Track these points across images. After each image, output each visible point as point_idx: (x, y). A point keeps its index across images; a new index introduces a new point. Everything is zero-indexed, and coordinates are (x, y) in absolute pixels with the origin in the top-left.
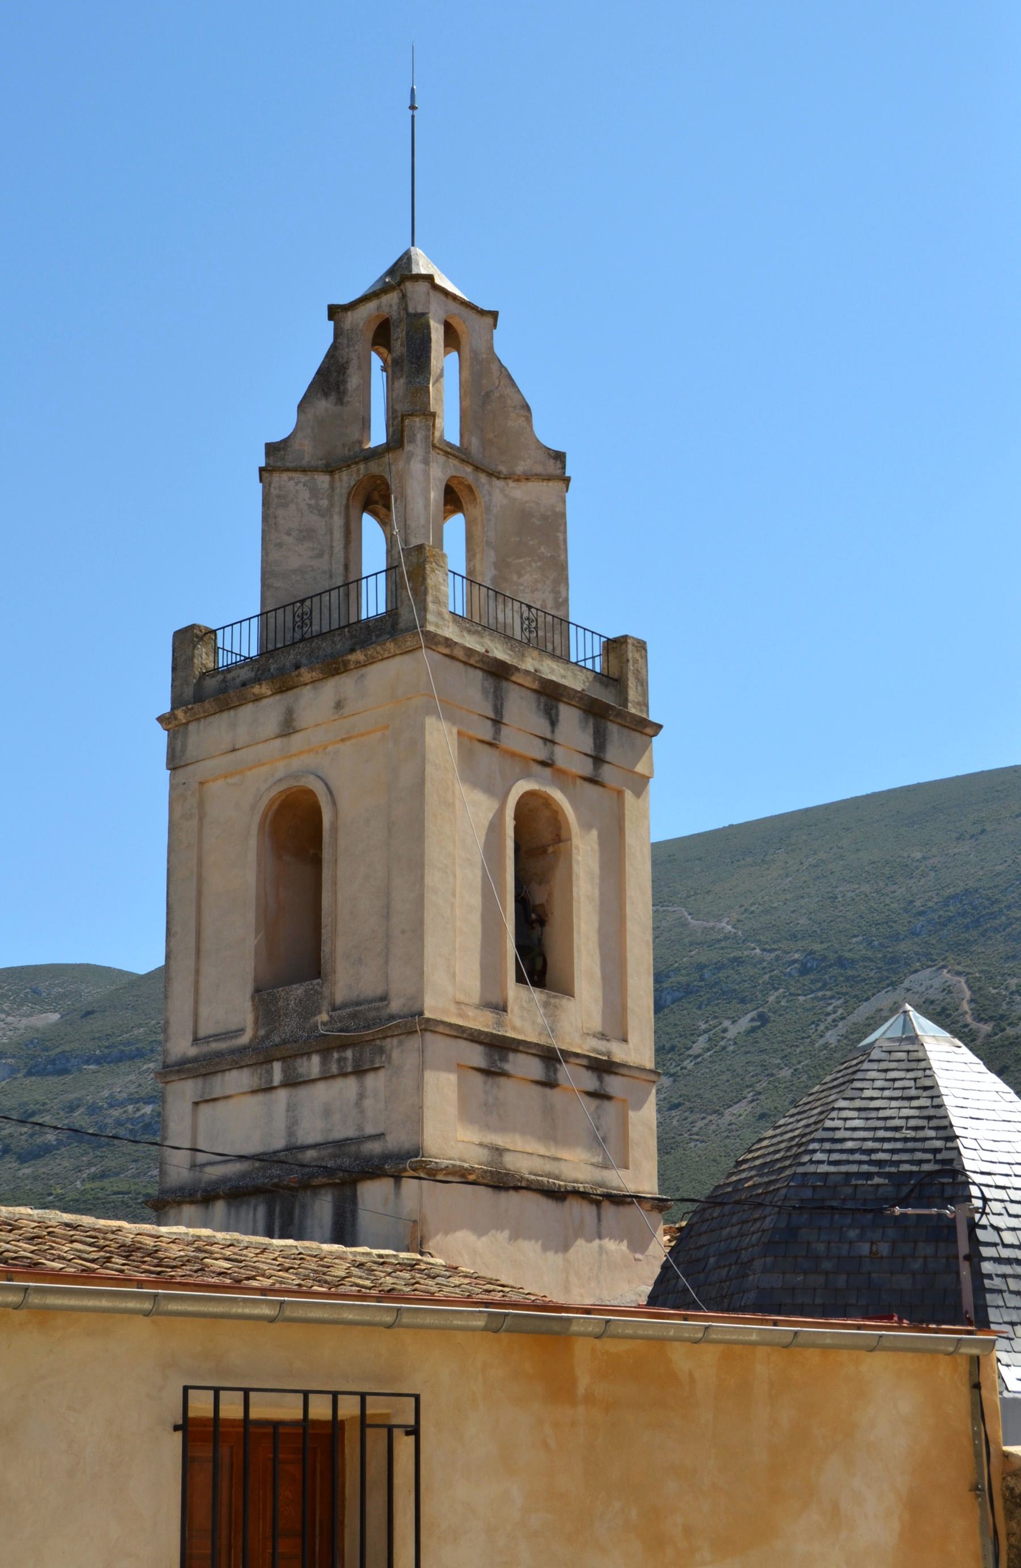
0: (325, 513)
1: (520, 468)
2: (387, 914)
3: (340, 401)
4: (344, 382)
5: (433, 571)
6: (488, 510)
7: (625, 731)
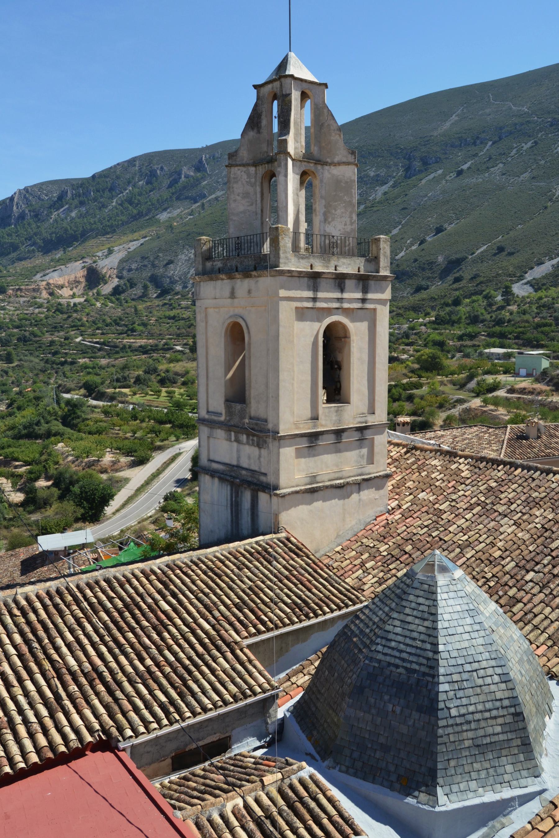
0: (253, 185)
1: (336, 160)
2: (267, 386)
3: (259, 132)
4: (260, 122)
5: (283, 238)
6: (321, 181)
7: (378, 282)
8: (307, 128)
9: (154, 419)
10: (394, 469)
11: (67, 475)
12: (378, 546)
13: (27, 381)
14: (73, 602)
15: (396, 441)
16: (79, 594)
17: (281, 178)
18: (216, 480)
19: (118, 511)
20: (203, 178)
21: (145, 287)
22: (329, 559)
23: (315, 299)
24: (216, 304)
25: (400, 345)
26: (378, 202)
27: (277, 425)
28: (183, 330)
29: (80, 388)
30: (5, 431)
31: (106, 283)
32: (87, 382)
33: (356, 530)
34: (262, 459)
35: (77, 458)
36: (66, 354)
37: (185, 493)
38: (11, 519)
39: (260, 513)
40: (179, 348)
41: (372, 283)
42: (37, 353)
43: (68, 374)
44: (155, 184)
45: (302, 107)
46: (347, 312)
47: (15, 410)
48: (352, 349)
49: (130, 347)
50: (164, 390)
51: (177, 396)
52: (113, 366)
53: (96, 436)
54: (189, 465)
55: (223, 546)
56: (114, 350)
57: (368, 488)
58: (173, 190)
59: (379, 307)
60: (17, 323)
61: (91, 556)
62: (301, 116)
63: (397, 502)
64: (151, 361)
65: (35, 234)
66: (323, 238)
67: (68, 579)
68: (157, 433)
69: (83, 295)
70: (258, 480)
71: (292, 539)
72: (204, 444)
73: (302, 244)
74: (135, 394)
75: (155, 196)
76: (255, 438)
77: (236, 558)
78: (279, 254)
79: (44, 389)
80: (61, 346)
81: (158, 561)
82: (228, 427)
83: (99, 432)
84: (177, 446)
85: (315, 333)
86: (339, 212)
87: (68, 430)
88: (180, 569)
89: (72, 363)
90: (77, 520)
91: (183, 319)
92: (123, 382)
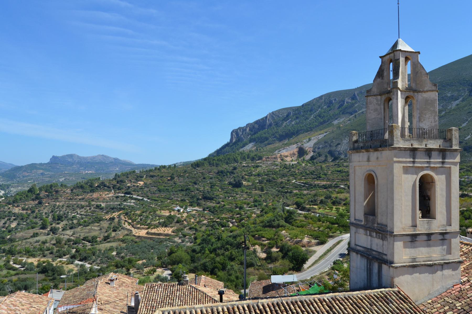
0: (379, 105)
1: (425, 89)
3: (382, 79)
6: (417, 101)
7: (452, 153)
8: (409, 75)
9: (329, 222)
10: (464, 259)
11: (286, 247)
12: (455, 303)
13: (270, 200)
14: (284, 311)
15: (466, 242)
16: (287, 307)
17: (394, 101)
18: (359, 256)
19: (310, 267)
20: (356, 103)
21: (326, 156)
22: (424, 307)
23: (414, 162)
24: (359, 165)
25: (469, 187)
26: (453, 110)
27: (393, 228)
28: (345, 178)
29: (294, 204)
30: (259, 223)
31: (307, 154)
32: (297, 202)
33: (441, 292)
34: (384, 246)
35: (291, 238)
36: (288, 188)
37: (344, 261)
38: (259, 266)
39: (383, 276)
40: (342, 186)
41: (448, 153)
42: (275, 187)
43: (289, 197)
44: (332, 107)
45: (406, 64)
46: (433, 169)
47: (264, 214)
48: (436, 189)
49: (318, 185)
50: (334, 207)
51: (341, 210)
52: (310, 194)
53: (301, 228)
54: (347, 246)
55: (362, 292)
56: (310, 187)
57: (448, 269)
58: (341, 109)
59: (452, 167)
60: (267, 173)
61: (296, 288)
62: (405, 69)
63: (467, 278)
64: (328, 192)
65: (276, 133)
66: (418, 130)
67: (282, 298)
68: (330, 229)
69: (296, 160)
70: (382, 258)
71: (401, 292)
72: (353, 236)
73: (407, 133)
74: (320, 208)
75: (331, 113)
76: (380, 235)
77: (369, 299)
78: (393, 139)
79: (277, 204)
80: (286, 184)
81: (327, 295)
82: (365, 228)
83: (302, 227)
84: (341, 236)
85: (414, 180)
86: (427, 116)
87: (287, 224)
88: (339, 301)
89: (291, 192)
90: (290, 270)
91: (345, 172)
92: (314, 202)
